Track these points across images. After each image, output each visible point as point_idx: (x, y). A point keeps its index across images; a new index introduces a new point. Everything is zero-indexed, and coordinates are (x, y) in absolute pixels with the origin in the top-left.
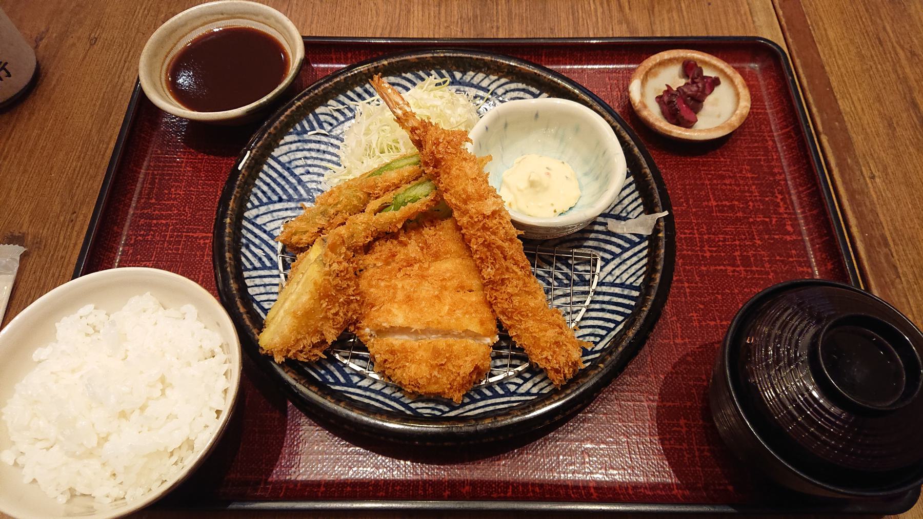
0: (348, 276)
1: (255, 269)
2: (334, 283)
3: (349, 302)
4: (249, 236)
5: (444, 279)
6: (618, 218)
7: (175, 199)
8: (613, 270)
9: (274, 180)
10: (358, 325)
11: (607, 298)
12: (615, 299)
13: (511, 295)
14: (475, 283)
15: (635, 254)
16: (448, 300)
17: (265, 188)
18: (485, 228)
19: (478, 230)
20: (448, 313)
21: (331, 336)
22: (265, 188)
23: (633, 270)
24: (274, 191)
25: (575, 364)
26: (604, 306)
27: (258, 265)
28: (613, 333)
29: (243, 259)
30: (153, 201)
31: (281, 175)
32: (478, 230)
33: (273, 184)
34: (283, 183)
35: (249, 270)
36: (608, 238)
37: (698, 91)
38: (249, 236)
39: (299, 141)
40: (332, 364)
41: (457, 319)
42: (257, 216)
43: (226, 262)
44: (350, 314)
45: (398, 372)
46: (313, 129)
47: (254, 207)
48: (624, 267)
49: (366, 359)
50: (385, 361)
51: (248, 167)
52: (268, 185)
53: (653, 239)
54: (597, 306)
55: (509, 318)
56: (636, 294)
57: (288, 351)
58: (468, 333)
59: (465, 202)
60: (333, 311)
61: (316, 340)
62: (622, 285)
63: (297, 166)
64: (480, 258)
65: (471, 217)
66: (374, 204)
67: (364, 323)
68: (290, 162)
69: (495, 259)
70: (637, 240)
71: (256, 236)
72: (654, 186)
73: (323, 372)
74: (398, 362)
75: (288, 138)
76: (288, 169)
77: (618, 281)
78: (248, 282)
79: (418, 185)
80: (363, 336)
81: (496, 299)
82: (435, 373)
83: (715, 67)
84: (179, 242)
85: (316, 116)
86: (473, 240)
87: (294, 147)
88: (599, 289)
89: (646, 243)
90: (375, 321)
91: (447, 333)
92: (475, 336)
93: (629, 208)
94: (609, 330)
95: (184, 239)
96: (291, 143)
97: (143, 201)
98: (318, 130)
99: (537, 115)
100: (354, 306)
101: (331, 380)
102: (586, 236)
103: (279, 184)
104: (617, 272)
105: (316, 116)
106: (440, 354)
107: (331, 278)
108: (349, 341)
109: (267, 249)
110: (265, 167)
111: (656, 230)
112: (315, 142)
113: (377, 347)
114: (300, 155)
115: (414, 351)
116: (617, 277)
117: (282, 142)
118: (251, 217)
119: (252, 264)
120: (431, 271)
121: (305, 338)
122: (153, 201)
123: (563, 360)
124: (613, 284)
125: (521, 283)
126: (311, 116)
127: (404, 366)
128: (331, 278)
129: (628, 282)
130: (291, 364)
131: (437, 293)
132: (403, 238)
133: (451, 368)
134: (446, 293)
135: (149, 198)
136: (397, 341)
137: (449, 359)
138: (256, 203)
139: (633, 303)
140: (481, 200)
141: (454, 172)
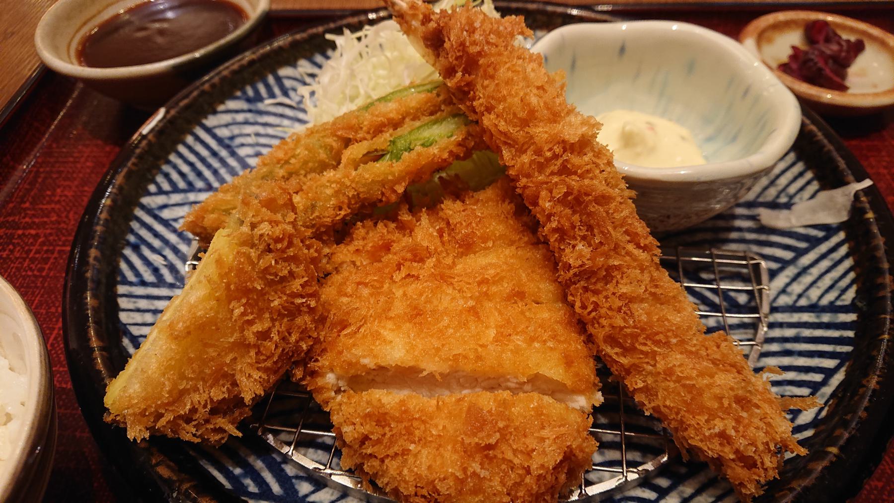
0: (291, 252)
1: (143, 283)
2: (262, 264)
3: (292, 312)
4: (144, 233)
5: (484, 282)
6: (774, 205)
7: (59, 202)
8: (788, 285)
9: (203, 160)
10: (311, 365)
11: (790, 333)
12: (807, 333)
13: (630, 299)
14: (546, 288)
15: (823, 257)
16: (495, 319)
17: (185, 169)
18: (565, 170)
19: (552, 173)
20: (496, 340)
21: (251, 385)
22: (185, 169)
23: (827, 281)
24: (199, 174)
25: (782, 447)
26: (789, 346)
27: (149, 277)
28: (828, 390)
29: (123, 266)
30: (27, 205)
31: (214, 154)
32: (552, 173)
33: (199, 166)
34: (216, 164)
35: (131, 284)
36: (763, 237)
37: (841, 51)
38: (144, 233)
39: (250, 111)
40: (259, 456)
41: (517, 351)
42: (165, 206)
43: (87, 263)
44: (293, 338)
45: (392, 466)
46: (272, 95)
47: (161, 192)
48: (807, 279)
49: (326, 448)
50: (365, 439)
51: (158, 132)
52: (191, 164)
53: (854, 227)
54: (775, 347)
55: (627, 351)
56: (851, 317)
57: (160, 416)
58: (538, 383)
59: (525, 123)
60: (258, 327)
61: (219, 394)
62: (813, 308)
63: (243, 145)
64: (559, 230)
65: (539, 152)
66: (356, 151)
67: (324, 362)
68: (232, 138)
69: (590, 228)
70: (821, 234)
71: (156, 235)
72: (830, 147)
73: (238, 471)
74: (392, 441)
75: (231, 104)
76: (228, 147)
77: (803, 302)
78: (123, 303)
79: (435, 122)
80: (320, 390)
81: (596, 306)
82: (475, 466)
83: (852, 30)
84: (46, 261)
85: (279, 80)
86: (544, 193)
87: (240, 117)
88: (773, 318)
89: (842, 235)
90: (347, 356)
91: (494, 382)
92: (556, 390)
93: (792, 189)
94: (815, 387)
95: (56, 255)
96: (237, 111)
97: (11, 205)
98: (282, 99)
99: (622, 50)
100: (304, 320)
101: (253, 488)
102: (723, 236)
103: (209, 166)
104: (797, 288)
105: (279, 80)
106: (484, 423)
107: (253, 253)
108: (292, 405)
109: (171, 256)
110: (190, 139)
111: (856, 210)
112: (275, 115)
113: (348, 411)
114: (249, 129)
115: (425, 419)
116: (800, 296)
117: (221, 108)
118: (153, 206)
119: (137, 274)
120: (459, 267)
121: (196, 389)
122: (27, 205)
123: (761, 437)
124: (793, 309)
125: (646, 277)
126: (271, 79)
127: (405, 452)
128: (253, 253)
129: (825, 301)
130: (160, 442)
131: (471, 303)
132: (405, 217)
133: (509, 455)
134: (489, 305)
135: (23, 202)
136: (388, 398)
137: (504, 438)
138: (166, 186)
139: (850, 334)
140: (555, 122)
141: (503, 73)
